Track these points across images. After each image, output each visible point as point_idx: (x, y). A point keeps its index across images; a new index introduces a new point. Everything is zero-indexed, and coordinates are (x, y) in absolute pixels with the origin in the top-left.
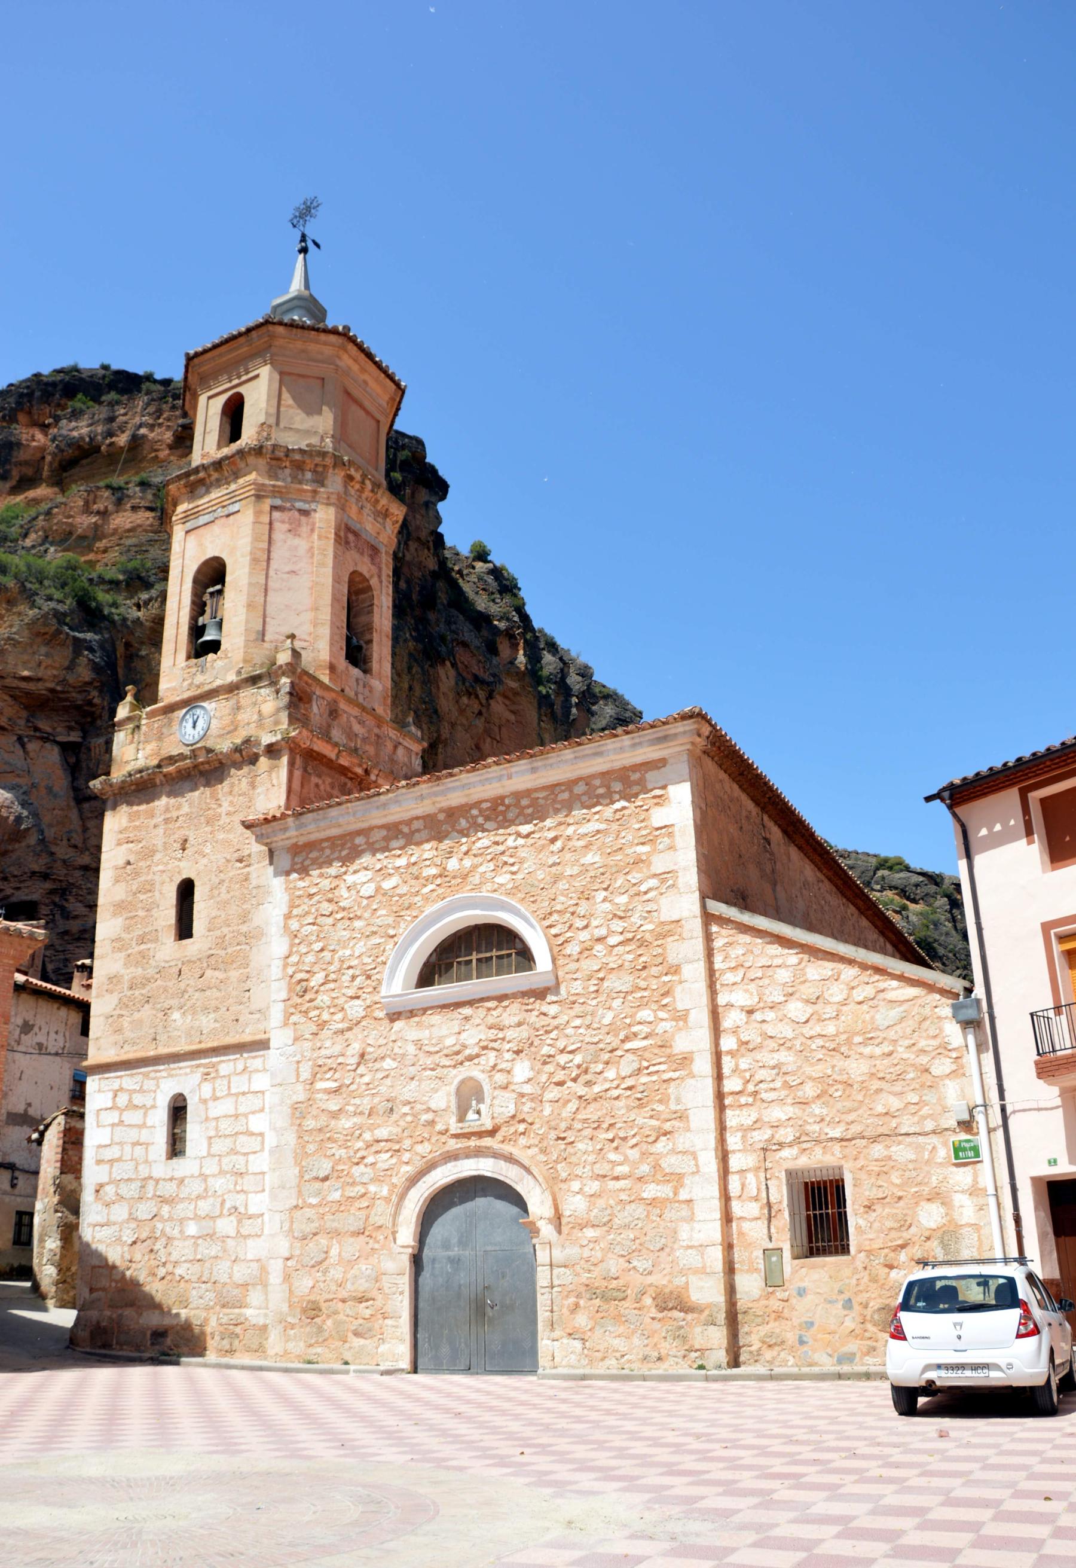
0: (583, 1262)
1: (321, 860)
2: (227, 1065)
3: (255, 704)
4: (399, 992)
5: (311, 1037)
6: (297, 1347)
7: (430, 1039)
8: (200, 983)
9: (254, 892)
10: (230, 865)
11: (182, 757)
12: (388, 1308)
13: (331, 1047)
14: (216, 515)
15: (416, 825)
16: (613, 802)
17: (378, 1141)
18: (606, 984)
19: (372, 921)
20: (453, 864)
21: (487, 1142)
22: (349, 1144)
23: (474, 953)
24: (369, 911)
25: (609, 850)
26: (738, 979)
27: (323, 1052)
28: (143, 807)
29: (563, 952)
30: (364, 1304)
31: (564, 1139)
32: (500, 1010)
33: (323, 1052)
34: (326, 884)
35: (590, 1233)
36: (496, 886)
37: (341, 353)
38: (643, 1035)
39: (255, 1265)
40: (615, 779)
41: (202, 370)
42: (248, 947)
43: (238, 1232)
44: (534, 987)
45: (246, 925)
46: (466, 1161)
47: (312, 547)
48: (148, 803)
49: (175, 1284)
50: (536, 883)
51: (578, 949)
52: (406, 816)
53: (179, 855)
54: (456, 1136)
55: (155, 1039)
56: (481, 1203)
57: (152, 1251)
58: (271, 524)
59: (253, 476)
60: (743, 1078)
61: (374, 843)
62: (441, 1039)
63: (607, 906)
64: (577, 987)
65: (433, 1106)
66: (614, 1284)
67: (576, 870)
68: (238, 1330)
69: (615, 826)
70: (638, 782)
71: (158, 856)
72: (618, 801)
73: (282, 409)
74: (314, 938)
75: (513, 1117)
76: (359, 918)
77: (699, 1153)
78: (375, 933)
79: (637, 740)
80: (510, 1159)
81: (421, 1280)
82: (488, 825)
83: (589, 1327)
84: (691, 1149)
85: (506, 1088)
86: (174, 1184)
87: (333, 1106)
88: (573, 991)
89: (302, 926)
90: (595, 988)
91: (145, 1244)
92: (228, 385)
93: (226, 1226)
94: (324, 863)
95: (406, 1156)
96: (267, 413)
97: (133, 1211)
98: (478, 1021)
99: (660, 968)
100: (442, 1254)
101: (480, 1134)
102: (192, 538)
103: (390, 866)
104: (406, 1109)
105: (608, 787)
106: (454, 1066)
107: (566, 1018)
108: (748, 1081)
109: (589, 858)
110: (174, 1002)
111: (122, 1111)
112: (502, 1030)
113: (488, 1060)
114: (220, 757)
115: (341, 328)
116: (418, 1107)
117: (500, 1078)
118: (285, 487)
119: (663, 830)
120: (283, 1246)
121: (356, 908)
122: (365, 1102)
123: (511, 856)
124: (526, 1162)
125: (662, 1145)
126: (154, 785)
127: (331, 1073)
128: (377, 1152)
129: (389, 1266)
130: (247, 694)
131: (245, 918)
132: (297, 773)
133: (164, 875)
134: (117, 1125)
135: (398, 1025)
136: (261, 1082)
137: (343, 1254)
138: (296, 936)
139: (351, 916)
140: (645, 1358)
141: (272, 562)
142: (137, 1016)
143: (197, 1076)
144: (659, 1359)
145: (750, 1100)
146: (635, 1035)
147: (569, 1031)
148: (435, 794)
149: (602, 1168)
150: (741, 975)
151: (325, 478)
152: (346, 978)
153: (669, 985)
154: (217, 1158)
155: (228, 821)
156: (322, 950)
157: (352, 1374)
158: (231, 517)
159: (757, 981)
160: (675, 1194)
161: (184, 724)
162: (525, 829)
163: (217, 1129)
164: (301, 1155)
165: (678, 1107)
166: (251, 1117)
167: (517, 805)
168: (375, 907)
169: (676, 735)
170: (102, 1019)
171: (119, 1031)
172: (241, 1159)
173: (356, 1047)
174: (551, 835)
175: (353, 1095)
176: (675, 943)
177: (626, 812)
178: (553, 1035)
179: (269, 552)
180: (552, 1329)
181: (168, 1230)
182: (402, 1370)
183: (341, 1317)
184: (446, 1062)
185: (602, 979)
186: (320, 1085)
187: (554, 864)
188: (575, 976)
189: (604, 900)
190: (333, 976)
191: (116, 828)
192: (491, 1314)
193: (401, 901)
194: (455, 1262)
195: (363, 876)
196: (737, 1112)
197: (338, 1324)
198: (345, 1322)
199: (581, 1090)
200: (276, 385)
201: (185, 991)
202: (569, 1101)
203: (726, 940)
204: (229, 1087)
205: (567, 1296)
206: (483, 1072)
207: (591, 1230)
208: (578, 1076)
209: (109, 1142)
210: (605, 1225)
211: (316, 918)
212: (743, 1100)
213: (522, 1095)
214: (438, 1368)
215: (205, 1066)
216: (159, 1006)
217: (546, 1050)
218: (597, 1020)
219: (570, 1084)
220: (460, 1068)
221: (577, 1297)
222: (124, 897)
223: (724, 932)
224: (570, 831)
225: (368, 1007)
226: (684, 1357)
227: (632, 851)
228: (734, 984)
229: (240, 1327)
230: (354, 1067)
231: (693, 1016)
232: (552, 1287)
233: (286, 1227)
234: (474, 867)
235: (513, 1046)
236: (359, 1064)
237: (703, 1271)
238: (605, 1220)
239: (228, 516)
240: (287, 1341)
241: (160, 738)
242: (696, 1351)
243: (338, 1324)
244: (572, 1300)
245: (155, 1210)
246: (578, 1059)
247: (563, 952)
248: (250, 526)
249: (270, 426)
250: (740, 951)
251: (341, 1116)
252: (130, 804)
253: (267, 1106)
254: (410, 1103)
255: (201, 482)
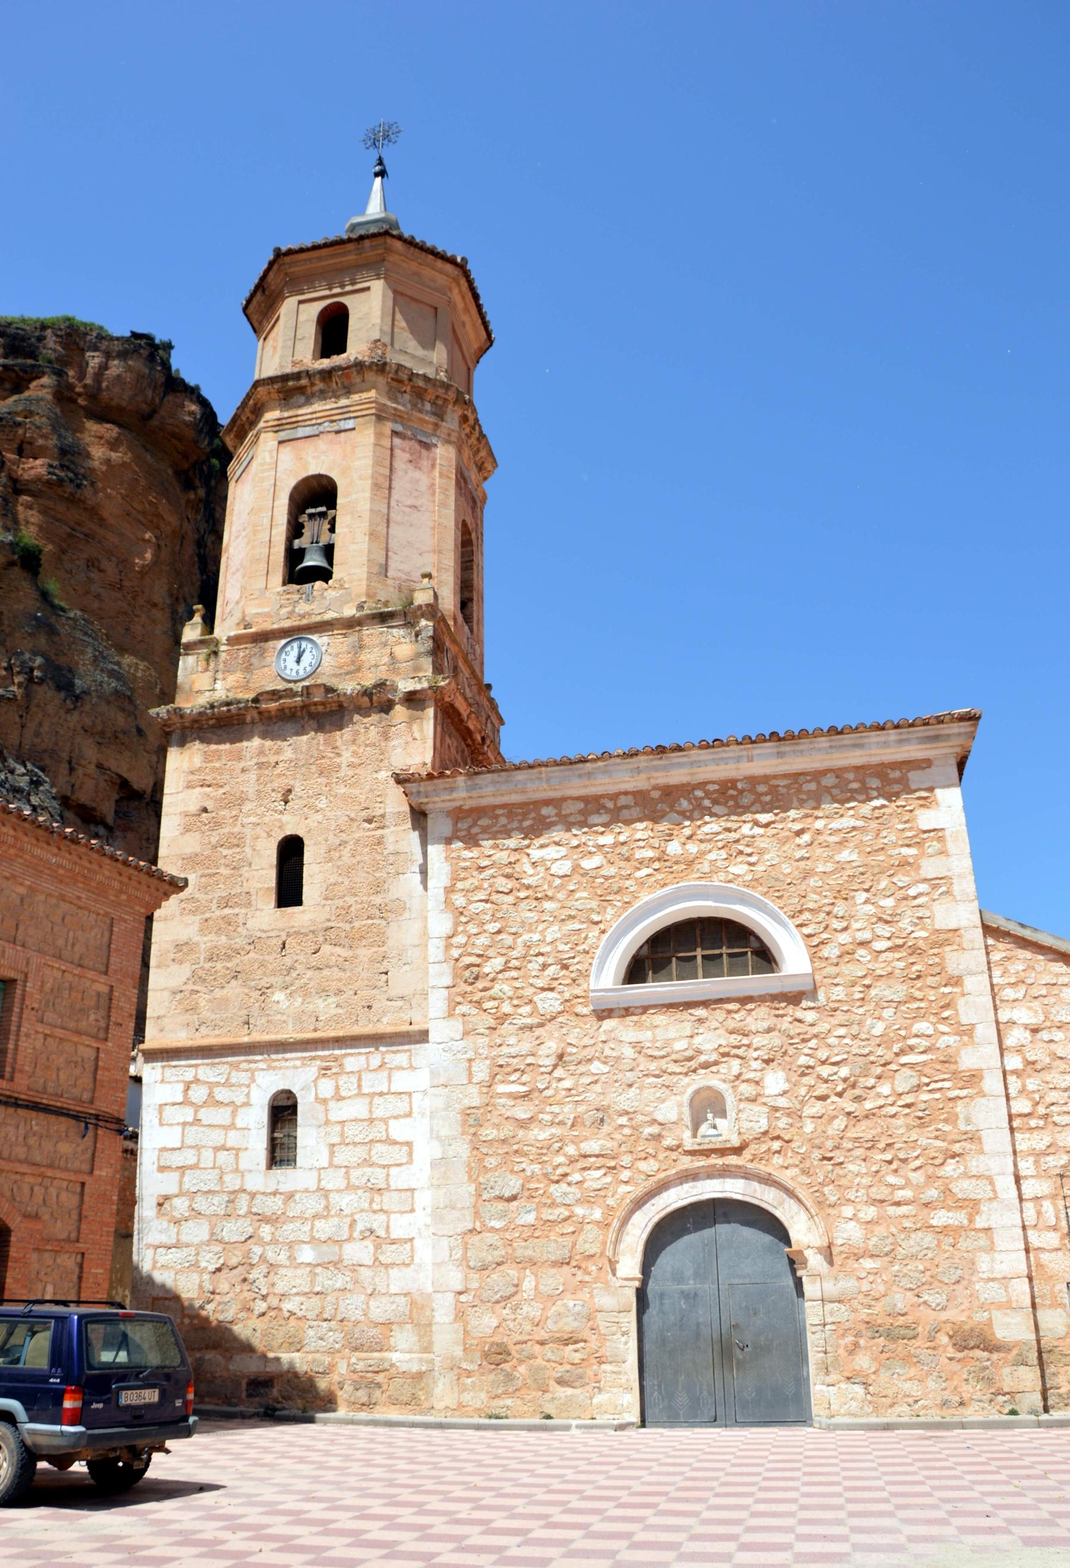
0: (861, 1296)
1: (495, 829)
2: (354, 1060)
3: (385, 644)
4: (610, 986)
5: (487, 1032)
6: (476, 1398)
7: (654, 1041)
8: (314, 960)
9: (391, 858)
10: (356, 824)
11: (290, 693)
12: (607, 1351)
13: (517, 1045)
14: (321, 428)
15: (623, 801)
16: (870, 799)
17: (585, 1156)
18: (873, 992)
19: (569, 904)
20: (674, 848)
21: (733, 1160)
22: (545, 1158)
23: (699, 950)
24: (565, 892)
25: (869, 849)
26: (1020, 995)
27: (505, 1050)
28: (227, 746)
29: (820, 954)
30: (571, 1347)
31: (830, 1159)
32: (743, 1013)
33: (505, 1050)
34: (502, 857)
35: (868, 1264)
36: (731, 877)
37: (454, 285)
38: (921, 1050)
39: (402, 1300)
40: (873, 775)
41: (293, 270)
42: (384, 923)
43: (376, 1259)
44: (786, 990)
45: (380, 896)
46: (708, 1181)
47: (433, 484)
48: (232, 742)
49: (282, 1322)
50: (781, 877)
51: (836, 952)
52: (613, 789)
53: (280, 806)
54: (692, 1153)
55: (248, 1023)
56: (723, 1230)
57: (245, 1280)
58: (392, 449)
59: (373, 394)
60: (1032, 1099)
61: (566, 816)
62: (668, 1042)
63: (870, 909)
64: (839, 993)
65: (660, 1118)
66: (901, 1320)
67: (829, 867)
68: (380, 1378)
69: (874, 825)
70: (897, 781)
71: (247, 807)
72: (876, 798)
73: (396, 330)
74: (488, 917)
75: (765, 1133)
76: (550, 898)
77: (995, 1178)
78: (574, 917)
79: (905, 737)
80: (768, 1180)
81: (646, 1317)
82: (716, 809)
83: (873, 1369)
84: (988, 1173)
85: (754, 1100)
86: (279, 1200)
87: (522, 1112)
88: (834, 998)
89: (470, 902)
90: (861, 995)
91: (235, 1272)
92: (327, 293)
93: (359, 1252)
94: (498, 832)
95: (625, 1175)
96: (381, 330)
97: (217, 1230)
98: (715, 1024)
99: (938, 978)
100: (673, 1287)
101: (722, 1152)
102: (286, 450)
103: (590, 843)
104: (623, 1120)
105: (863, 783)
106: (686, 1074)
107: (827, 1026)
108: (1038, 1103)
109: (845, 855)
110: (277, 980)
111: (197, 1108)
112: (747, 1035)
113: (730, 1068)
114: (342, 699)
115: (459, 260)
116: (640, 1118)
117: (746, 1089)
118: (407, 413)
119: (932, 834)
120: (455, 1278)
121: (546, 887)
122: (565, 1110)
123: (748, 846)
124: (790, 1184)
125: (951, 1168)
126: (244, 723)
127: (517, 1075)
128: (584, 1169)
129: (605, 1301)
130: (372, 633)
131: (378, 887)
132: (439, 729)
133: (258, 828)
134: (191, 1124)
135: (608, 1024)
136: (402, 1081)
137: (541, 1287)
138: (461, 913)
139: (539, 895)
140: (945, 1403)
141: (393, 491)
142: (218, 993)
143: (312, 1071)
144: (962, 1404)
145: (1041, 1123)
146: (912, 1048)
147: (831, 1040)
148: (656, 769)
149: (882, 1192)
150: (1023, 992)
151: (445, 413)
152: (534, 966)
153: (950, 997)
154: (343, 1170)
155: (351, 773)
156: (499, 932)
157: (574, 1431)
158: (343, 434)
159: (1041, 999)
160: (971, 1221)
161: (283, 656)
162: (764, 818)
163: (342, 1135)
164: (477, 1169)
165: (969, 1128)
166: (392, 1122)
167: (753, 791)
168: (572, 888)
169: (949, 736)
170: (166, 994)
171: (193, 1009)
172: (380, 1173)
173: (552, 1046)
174: (797, 826)
175: (547, 1101)
176: (955, 953)
177: (886, 811)
178: (813, 1043)
179: (391, 480)
180: (827, 1373)
181: (270, 1255)
182: (633, 1424)
183: (539, 1361)
184: (677, 1069)
185: (868, 987)
186: (501, 1088)
187: (802, 859)
188: (835, 981)
189: (867, 902)
190: (514, 963)
191: (186, 766)
192: (741, 1357)
193: (607, 884)
194: (691, 1297)
195: (552, 852)
196: (1027, 1135)
197: (535, 1371)
198: (545, 1368)
199: (850, 1107)
200: (390, 303)
201: (292, 968)
202: (836, 1117)
203: (1004, 954)
204: (359, 1086)
205: (843, 1335)
206: (724, 1081)
207: (870, 1260)
208: (844, 1090)
209: (179, 1145)
210: (887, 1255)
211: (490, 895)
212: (1033, 1123)
213: (776, 1109)
214: (673, 1420)
215: (322, 1058)
216: (253, 983)
217: (803, 1060)
218: (865, 1030)
219: (834, 1098)
220: (694, 1076)
221: (855, 1336)
222: (198, 849)
223: (1000, 946)
224: (819, 824)
225: (567, 1001)
226: (991, 1401)
227: (897, 851)
228: (1014, 1001)
229: (382, 1375)
230: (550, 1069)
231: (979, 1031)
232: (825, 1325)
233: (458, 1254)
234: (702, 854)
235: (763, 1054)
236: (555, 1066)
237: (1008, 1306)
238: (887, 1249)
239: (338, 432)
240: (461, 1392)
241: (248, 668)
242: (1004, 1395)
243: (535, 1371)
244: (850, 1339)
245: (250, 1230)
246: (844, 1072)
247: (820, 954)
248: (371, 449)
249: (385, 345)
250: (1021, 967)
251: (532, 1126)
252: (204, 740)
253: (415, 1110)
254: (627, 1113)
255: (301, 390)
